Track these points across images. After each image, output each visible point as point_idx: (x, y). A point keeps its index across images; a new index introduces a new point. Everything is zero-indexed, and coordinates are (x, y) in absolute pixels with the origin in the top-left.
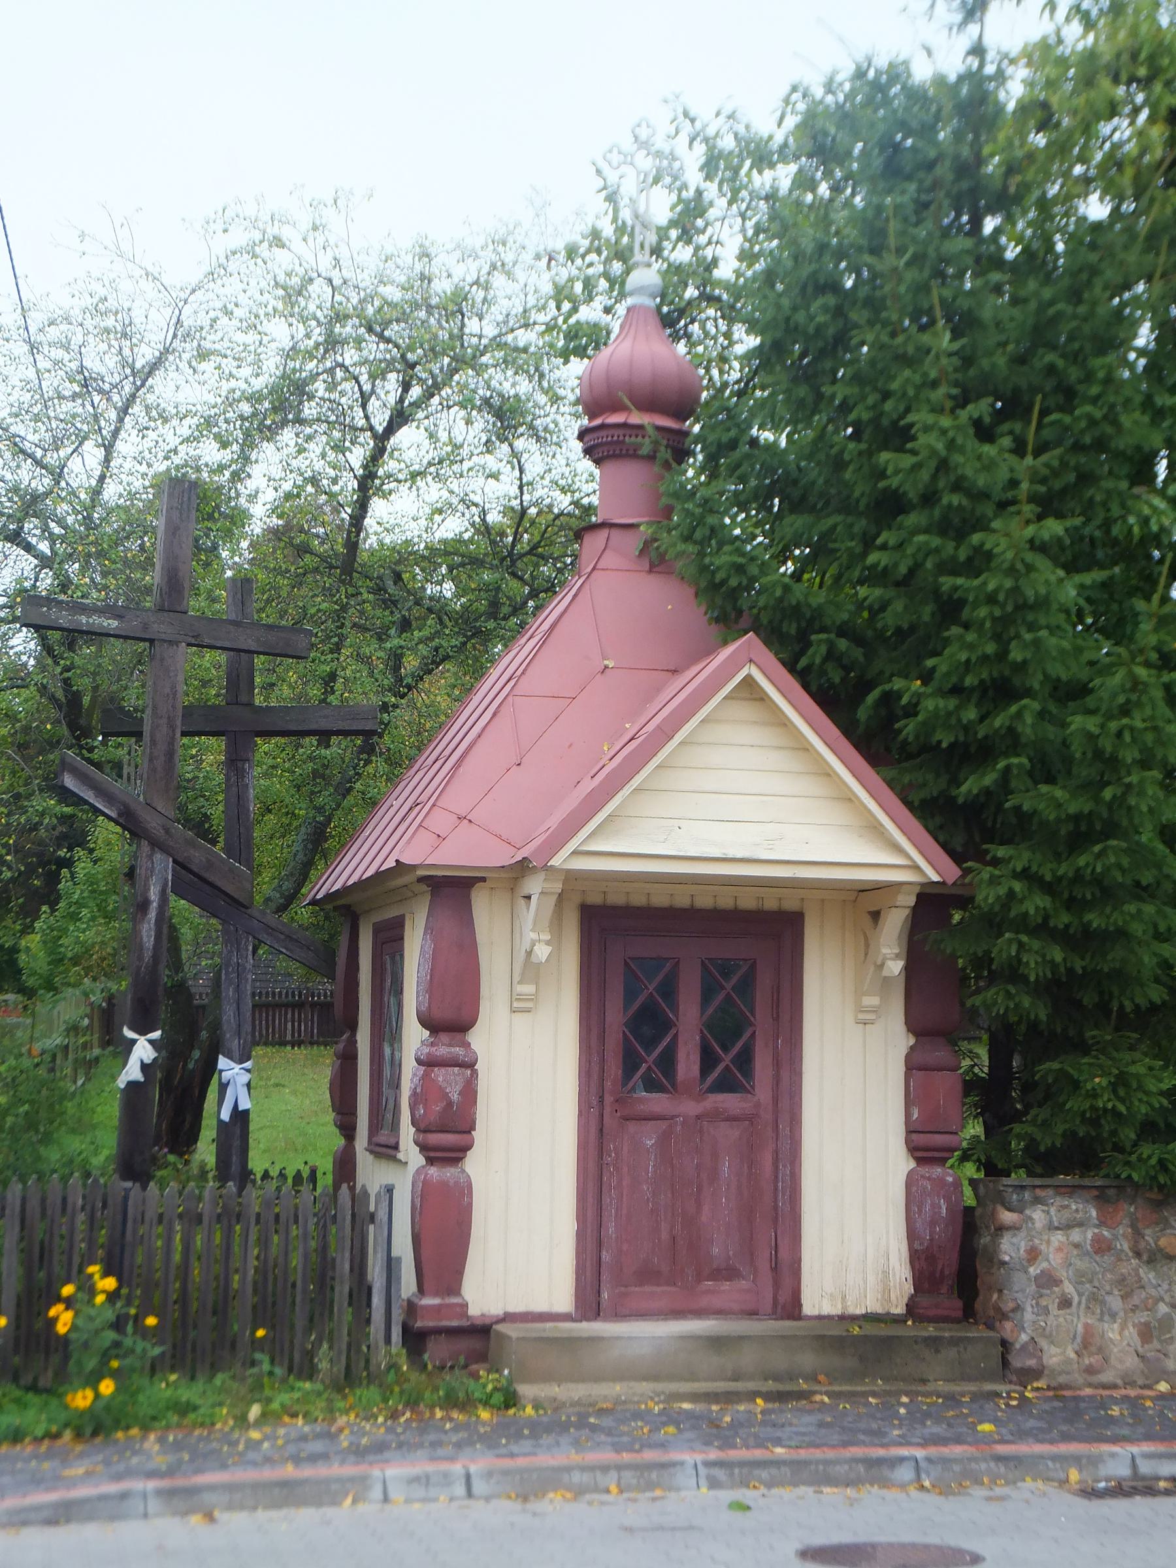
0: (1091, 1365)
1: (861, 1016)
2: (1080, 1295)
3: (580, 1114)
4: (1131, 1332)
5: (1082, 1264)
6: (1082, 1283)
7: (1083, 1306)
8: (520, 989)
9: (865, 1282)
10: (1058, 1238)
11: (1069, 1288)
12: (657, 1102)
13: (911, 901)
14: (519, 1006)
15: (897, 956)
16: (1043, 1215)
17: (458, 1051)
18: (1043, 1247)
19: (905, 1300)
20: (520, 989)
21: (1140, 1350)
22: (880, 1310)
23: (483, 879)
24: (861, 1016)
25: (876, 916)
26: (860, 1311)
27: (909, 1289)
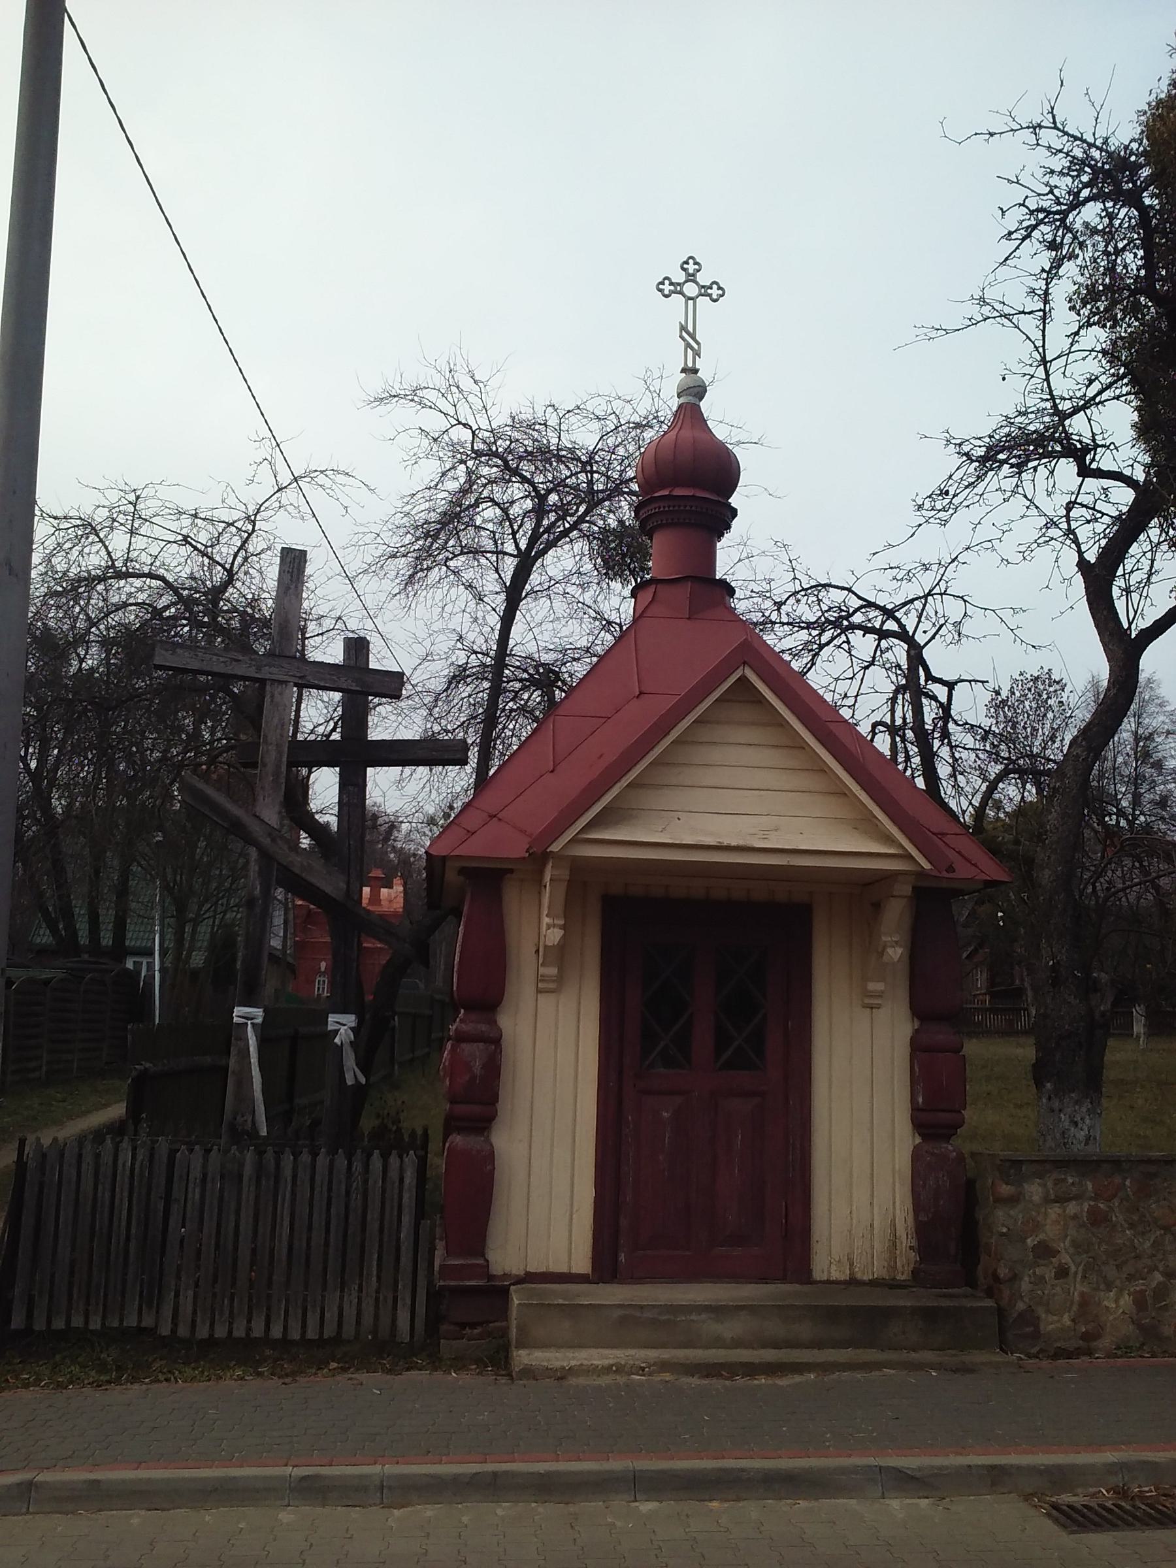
0: (1087, 1332)
1: (867, 1001)
2: (1077, 1266)
4: (1126, 1301)
6: (1079, 1253)
7: (1080, 1275)
8: (542, 970)
9: (872, 1247)
10: (1054, 1211)
11: (1066, 1258)
13: (907, 890)
14: (549, 987)
16: (1040, 1189)
17: (483, 1027)
20: (542, 970)
21: (1135, 1317)
23: (511, 871)
24: (867, 1001)
25: (877, 906)
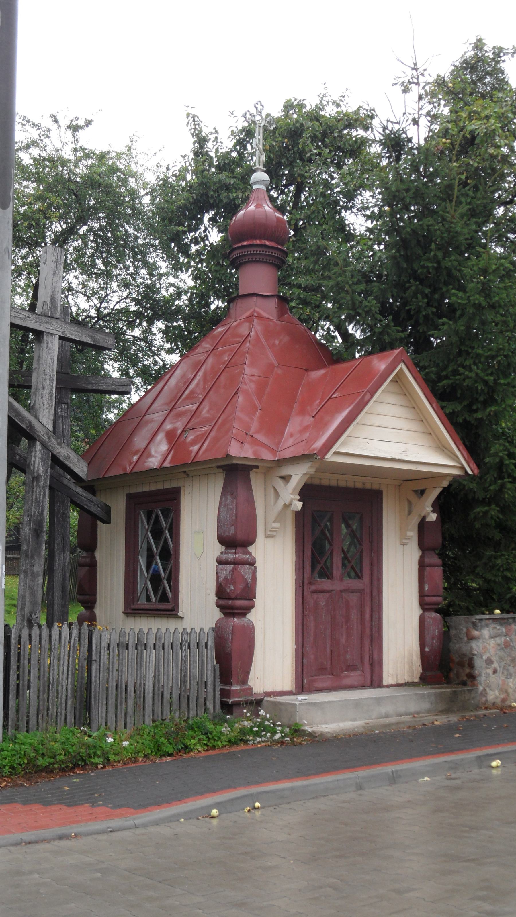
2: (500, 667)
3: (296, 591)
5: (501, 653)
12: (326, 584)
15: (433, 511)
18: (488, 646)
19: (419, 675)
22: (410, 681)
25: (422, 492)
26: (402, 682)
27: (420, 670)
